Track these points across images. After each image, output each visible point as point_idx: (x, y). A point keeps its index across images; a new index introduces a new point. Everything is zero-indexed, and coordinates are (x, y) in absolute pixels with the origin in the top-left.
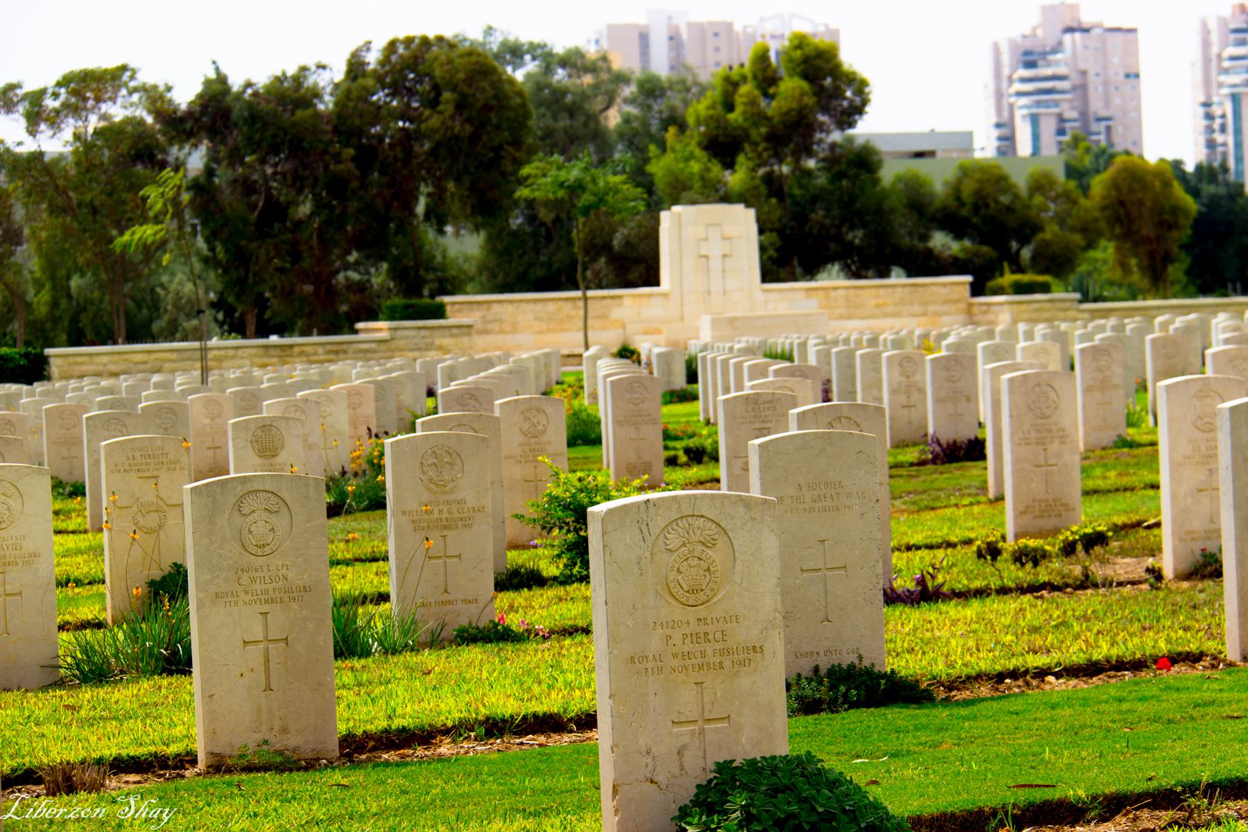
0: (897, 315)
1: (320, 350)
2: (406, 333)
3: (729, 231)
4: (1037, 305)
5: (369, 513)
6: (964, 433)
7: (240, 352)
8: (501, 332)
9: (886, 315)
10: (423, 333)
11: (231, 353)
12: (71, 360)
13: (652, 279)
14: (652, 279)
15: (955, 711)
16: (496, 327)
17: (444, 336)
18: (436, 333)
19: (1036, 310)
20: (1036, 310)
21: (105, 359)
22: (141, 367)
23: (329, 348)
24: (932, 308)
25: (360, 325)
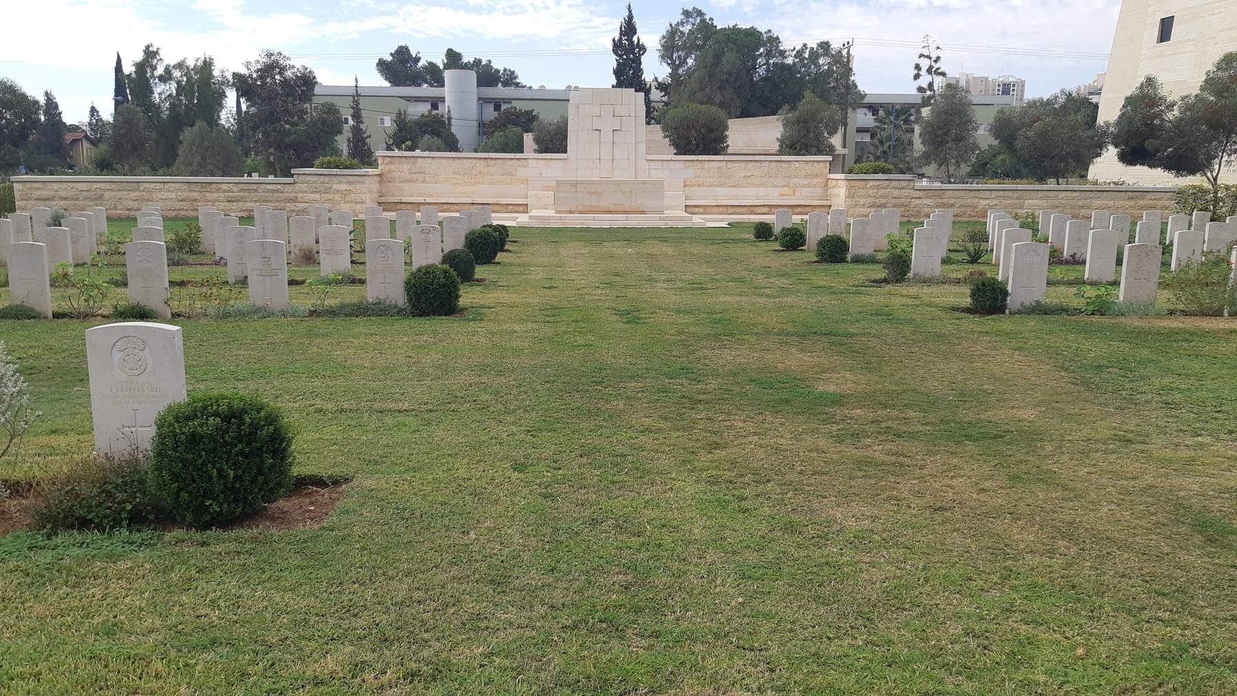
0: (764, 185)
1: (235, 188)
2: (308, 178)
3: (620, 110)
4: (878, 183)
5: (37, 308)
6: (294, 288)
7: (167, 186)
8: (424, 181)
9: (753, 185)
10: (322, 179)
11: (161, 186)
12: (28, 185)
13: (564, 150)
14: (564, 150)
15: (952, 267)
16: (420, 177)
17: (340, 183)
18: (334, 179)
19: (877, 187)
20: (877, 187)
21: (56, 186)
22: (85, 194)
23: (241, 186)
24: (793, 181)
25: (293, 171)
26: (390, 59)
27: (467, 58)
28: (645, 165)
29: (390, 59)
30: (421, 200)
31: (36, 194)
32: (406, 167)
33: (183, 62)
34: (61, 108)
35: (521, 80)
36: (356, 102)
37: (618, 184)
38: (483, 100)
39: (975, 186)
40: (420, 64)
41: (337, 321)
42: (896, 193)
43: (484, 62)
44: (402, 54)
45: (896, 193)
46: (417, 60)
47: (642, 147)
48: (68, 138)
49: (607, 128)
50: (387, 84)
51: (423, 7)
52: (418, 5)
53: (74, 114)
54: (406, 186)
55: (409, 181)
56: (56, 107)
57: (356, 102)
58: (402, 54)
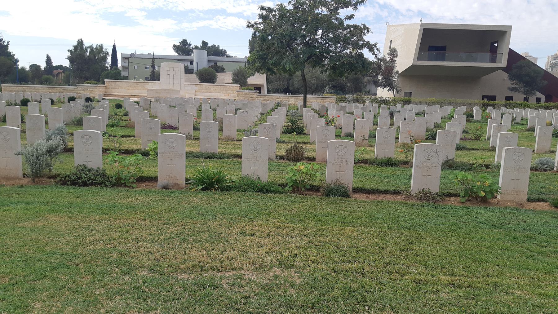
0: (219, 93)
13: (159, 80)
16: (117, 87)
26: (179, 44)
27: (210, 45)
28: (183, 85)
29: (179, 44)
30: (116, 94)
31: (8, 89)
32: (113, 84)
33: (92, 46)
34: (52, 61)
35: (228, 53)
36: (153, 62)
37: (165, 90)
38: (209, 61)
39: (316, 96)
40: (191, 47)
41: (537, 173)
42: (252, 96)
43: (217, 46)
44: (184, 42)
45: (252, 96)
46: (190, 45)
47: (183, 80)
48: (55, 72)
49: (172, 74)
50: (177, 54)
51: (224, 17)
52: (222, 16)
53: (20, 65)
54: (113, 90)
55: (114, 88)
56: (51, 60)
57: (153, 62)
58: (184, 42)
